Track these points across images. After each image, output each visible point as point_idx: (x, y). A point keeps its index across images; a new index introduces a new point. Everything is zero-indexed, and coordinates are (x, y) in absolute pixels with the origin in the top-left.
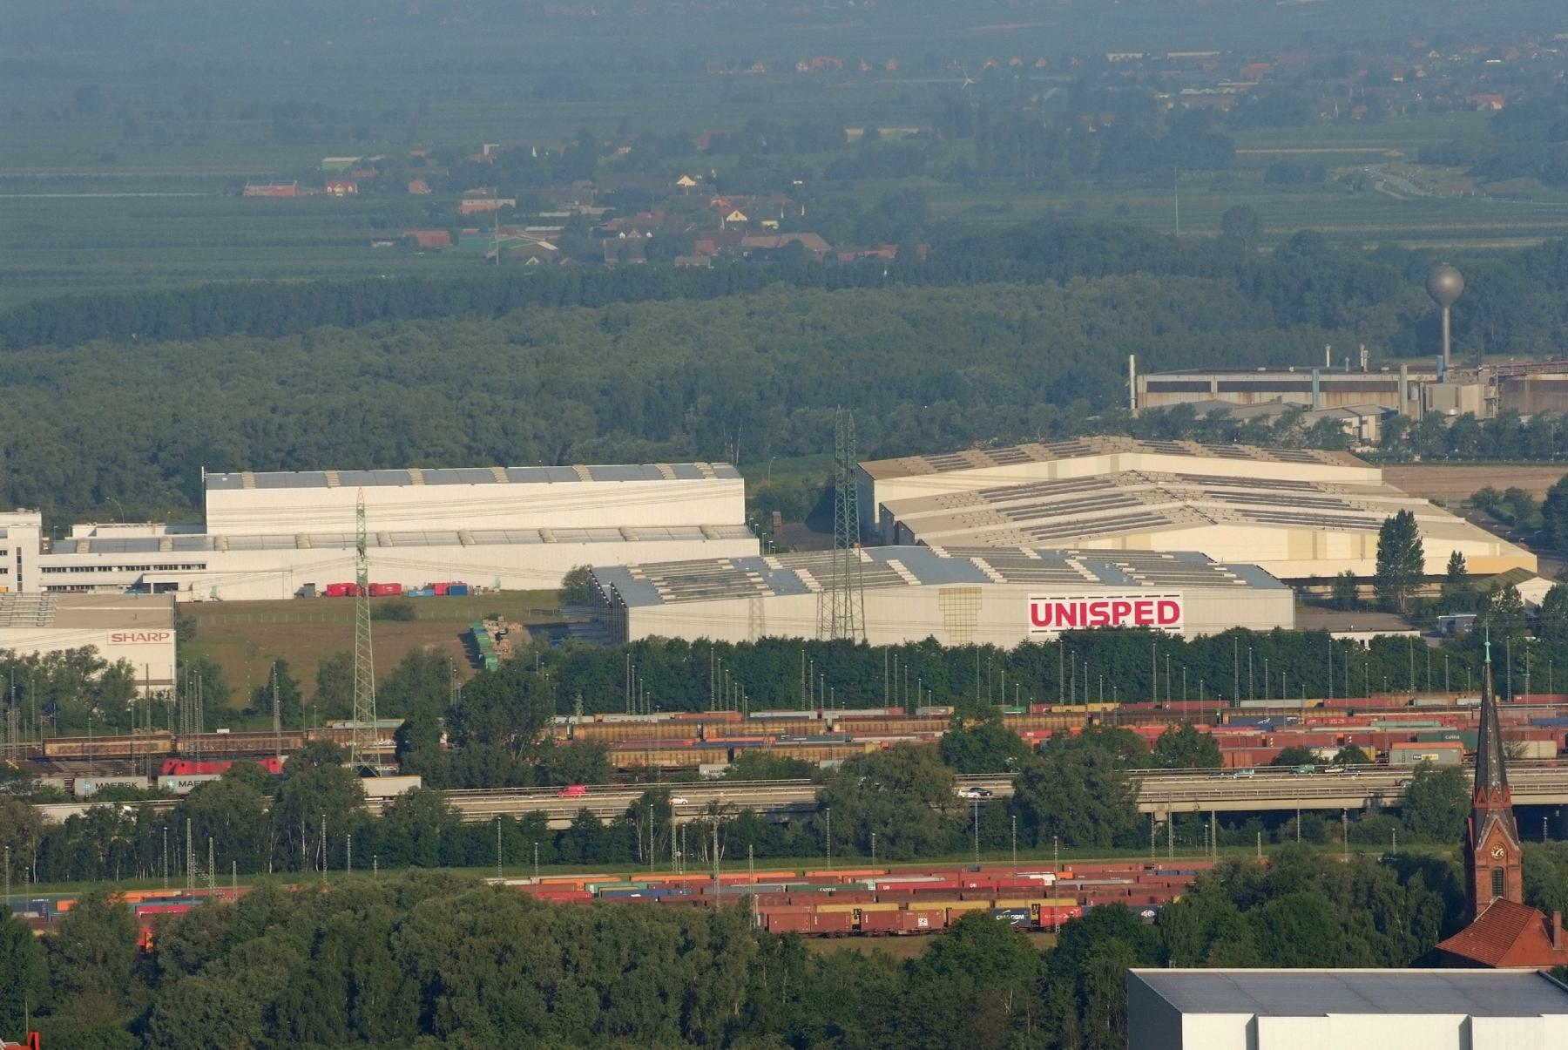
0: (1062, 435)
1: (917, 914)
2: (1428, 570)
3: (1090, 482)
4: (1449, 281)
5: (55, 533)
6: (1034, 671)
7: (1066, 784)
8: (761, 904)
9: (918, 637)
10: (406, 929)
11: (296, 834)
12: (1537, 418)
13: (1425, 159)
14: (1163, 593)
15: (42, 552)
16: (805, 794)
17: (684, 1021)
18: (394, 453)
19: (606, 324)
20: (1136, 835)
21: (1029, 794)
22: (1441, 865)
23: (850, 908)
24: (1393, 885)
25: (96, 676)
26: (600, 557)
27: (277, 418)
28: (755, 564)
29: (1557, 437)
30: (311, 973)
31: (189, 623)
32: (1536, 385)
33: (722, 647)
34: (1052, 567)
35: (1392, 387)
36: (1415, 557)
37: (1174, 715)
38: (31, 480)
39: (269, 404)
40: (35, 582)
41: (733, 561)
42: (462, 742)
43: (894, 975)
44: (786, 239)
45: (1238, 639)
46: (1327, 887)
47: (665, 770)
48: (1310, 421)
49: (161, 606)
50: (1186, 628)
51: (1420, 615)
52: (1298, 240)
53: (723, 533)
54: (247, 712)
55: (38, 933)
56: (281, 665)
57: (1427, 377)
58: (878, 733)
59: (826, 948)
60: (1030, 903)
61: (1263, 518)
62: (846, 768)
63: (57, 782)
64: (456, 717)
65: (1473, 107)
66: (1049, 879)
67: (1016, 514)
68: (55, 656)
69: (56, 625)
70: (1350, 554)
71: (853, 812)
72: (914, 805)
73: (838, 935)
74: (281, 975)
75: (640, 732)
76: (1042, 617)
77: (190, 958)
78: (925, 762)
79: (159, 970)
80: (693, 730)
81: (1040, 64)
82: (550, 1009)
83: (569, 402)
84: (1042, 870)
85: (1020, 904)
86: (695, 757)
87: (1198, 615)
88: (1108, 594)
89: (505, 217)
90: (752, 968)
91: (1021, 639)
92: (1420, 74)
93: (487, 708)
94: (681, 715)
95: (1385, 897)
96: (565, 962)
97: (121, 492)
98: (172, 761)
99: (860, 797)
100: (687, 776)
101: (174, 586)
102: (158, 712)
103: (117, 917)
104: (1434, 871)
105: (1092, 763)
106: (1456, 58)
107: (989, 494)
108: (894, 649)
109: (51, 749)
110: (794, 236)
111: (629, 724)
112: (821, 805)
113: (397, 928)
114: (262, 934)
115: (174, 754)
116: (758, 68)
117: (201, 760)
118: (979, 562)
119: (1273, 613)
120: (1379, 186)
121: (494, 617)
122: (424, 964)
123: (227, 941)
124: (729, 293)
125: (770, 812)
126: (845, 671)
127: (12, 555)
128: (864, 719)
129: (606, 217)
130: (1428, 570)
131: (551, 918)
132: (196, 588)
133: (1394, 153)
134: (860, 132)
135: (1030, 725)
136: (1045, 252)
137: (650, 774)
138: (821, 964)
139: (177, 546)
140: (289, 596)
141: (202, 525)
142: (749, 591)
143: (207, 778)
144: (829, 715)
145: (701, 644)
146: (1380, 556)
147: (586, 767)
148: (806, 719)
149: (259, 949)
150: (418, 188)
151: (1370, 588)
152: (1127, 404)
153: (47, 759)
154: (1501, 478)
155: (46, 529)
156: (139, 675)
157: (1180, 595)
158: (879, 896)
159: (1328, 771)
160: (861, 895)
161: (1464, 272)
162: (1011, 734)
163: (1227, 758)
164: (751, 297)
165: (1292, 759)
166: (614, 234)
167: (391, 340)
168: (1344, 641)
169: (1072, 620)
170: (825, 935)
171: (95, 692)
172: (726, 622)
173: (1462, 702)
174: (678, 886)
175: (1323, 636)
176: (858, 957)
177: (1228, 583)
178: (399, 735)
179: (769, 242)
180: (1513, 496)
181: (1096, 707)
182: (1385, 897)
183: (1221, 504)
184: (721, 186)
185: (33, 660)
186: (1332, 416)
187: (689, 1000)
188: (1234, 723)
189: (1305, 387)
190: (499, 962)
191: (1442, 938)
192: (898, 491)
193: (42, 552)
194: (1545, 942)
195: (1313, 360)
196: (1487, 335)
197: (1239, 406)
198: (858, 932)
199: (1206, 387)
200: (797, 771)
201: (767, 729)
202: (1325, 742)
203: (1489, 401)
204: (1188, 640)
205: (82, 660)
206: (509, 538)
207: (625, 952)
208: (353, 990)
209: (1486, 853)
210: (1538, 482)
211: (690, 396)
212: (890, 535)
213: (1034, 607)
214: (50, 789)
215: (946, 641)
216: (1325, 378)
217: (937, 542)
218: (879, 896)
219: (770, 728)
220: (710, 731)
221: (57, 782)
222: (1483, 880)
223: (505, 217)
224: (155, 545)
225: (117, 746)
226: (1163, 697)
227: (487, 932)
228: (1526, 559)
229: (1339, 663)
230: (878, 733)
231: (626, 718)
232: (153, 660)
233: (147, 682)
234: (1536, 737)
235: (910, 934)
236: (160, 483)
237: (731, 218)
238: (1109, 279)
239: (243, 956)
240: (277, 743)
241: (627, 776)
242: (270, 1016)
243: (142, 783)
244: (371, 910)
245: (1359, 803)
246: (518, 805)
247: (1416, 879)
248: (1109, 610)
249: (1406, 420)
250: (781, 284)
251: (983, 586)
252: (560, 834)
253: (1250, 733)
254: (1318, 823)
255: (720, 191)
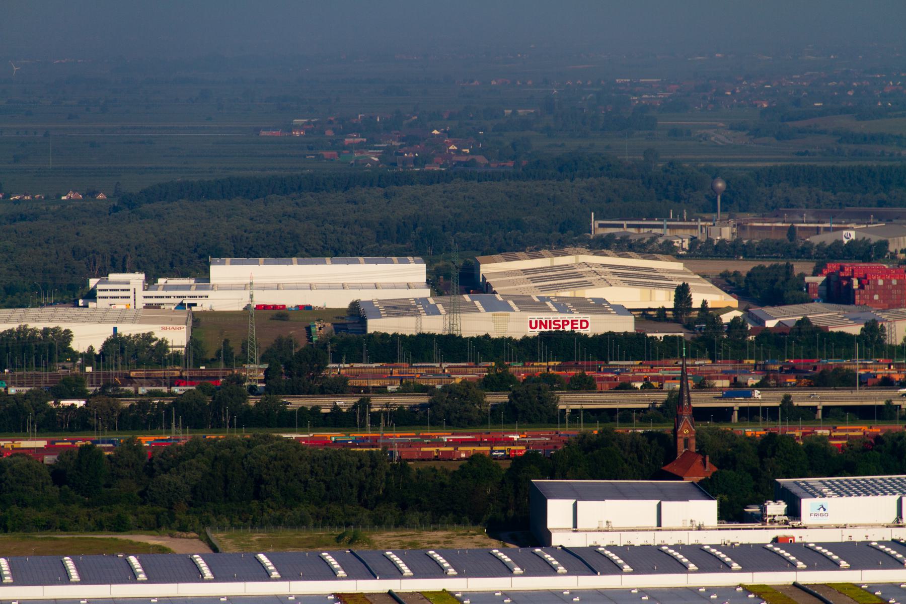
0: (559, 246)
1: (461, 452)
2: (694, 306)
3: (566, 267)
4: (720, 185)
5: (150, 282)
6: (527, 348)
7: (529, 398)
8: (399, 447)
9: (482, 334)
10: (249, 457)
11: (220, 414)
12: (750, 242)
13: (731, 129)
14: (582, 317)
15: (144, 290)
16: (425, 399)
17: (359, 496)
18: (293, 249)
19: (386, 195)
20: (556, 418)
21: (514, 401)
22: (666, 436)
23: (434, 449)
24: (646, 444)
25: (153, 344)
26: (364, 296)
27: (246, 235)
28: (424, 301)
29: (758, 249)
30: (211, 474)
31: (199, 322)
32: (752, 228)
33: (403, 336)
34: (541, 305)
35: (696, 227)
36: (689, 301)
37: (581, 367)
38: (145, 259)
39: (243, 228)
40: (141, 303)
41: (415, 299)
42: (291, 376)
43: (448, 478)
44: (470, 157)
45: (610, 337)
46: (620, 444)
47: (373, 387)
48: (661, 240)
49: (183, 315)
50: (590, 332)
51: (689, 326)
52: (671, 163)
53: (417, 286)
54: (213, 360)
55: (107, 453)
56: (226, 342)
57: (709, 223)
58: (461, 374)
59: (423, 466)
60: (507, 448)
61: (632, 284)
62: (444, 389)
63: (131, 389)
64: (288, 366)
65: (756, 106)
66: (516, 437)
67: (534, 280)
68: (138, 336)
69: (140, 323)
70: (664, 299)
71: (443, 408)
72: (468, 406)
73: (429, 460)
74: (199, 475)
75: (365, 372)
76: (534, 326)
77: (165, 467)
78: (473, 387)
79: (154, 471)
80: (388, 371)
81: (589, 83)
82: (306, 490)
83: (365, 229)
84: (514, 434)
85: (502, 448)
86: (387, 382)
87: (596, 325)
88: (560, 317)
89: (360, 147)
90: (388, 475)
91: (523, 335)
92: (738, 91)
93: (301, 363)
94: (385, 364)
95: (642, 448)
96: (312, 472)
97: (181, 263)
98: (179, 381)
99: (447, 402)
100: (381, 391)
101: (195, 305)
102: (176, 358)
103: (137, 449)
104: (660, 437)
105: (539, 389)
106: (754, 84)
107: (525, 271)
108: (472, 338)
109: (133, 374)
110: (474, 157)
111: (363, 368)
112: (431, 404)
113: (246, 457)
114: (193, 458)
115: (181, 377)
116: (476, 83)
117: (191, 381)
118: (511, 303)
119: (626, 325)
120: (713, 138)
121: (319, 320)
122: (256, 471)
123: (182, 459)
124: (438, 182)
125: (411, 407)
126: (451, 347)
127: (132, 291)
128: (458, 367)
129: (401, 147)
130: (694, 306)
131: (308, 454)
132: (203, 305)
133: (721, 124)
134: (510, 111)
135: (519, 370)
136: (568, 167)
137: (367, 390)
138: (419, 472)
139: (197, 289)
140: (241, 309)
141: (208, 280)
142: (416, 314)
143: (191, 388)
144: (444, 365)
145: (395, 335)
146: (675, 300)
147: (338, 387)
148: (434, 367)
149: (191, 464)
150: (329, 133)
151: (670, 312)
152: (590, 232)
153: (132, 378)
154: (744, 267)
155: (147, 279)
156: (170, 344)
157: (589, 317)
158: (448, 444)
159: (635, 393)
160: (440, 443)
161: (728, 182)
162: (512, 376)
163: (599, 386)
164: (446, 185)
165: (625, 387)
166: (402, 154)
167: (299, 201)
168: (652, 338)
169: (546, 327)
170: (423, 460)
171: (152, 350)
172: (406, 326)
173: (697, 363)
174: (367, 438)
175: (644, 335)
176: (434, 470)
177: (609, 313)
178: (266, 372)
179: (463, 159)
180: (736, 274)
181: (551, 363)
182: (642, 448)
183: (616, 277)
184: (449, 134)
185: (129, 337)
186: (669, 239)
187: (361, 488)
188: (606, 371)
189: (661, 227)
190: (285, 471)
191: (664, 465)
192: (490, 269)
193: (144, 290)
194: (702, 468)
195: (664, 216)
196: (740, 205)
197: (634, 234)
198: (437, 458)
199: (622, 226)
200: (424, 390)
201: (419, 372)
202: (638, 379)
203: (733, 234)
204: (590, 336)
205: (148, 337)
206: (330, 287)
207: (336, 468)
208: (226, 481)
209: (682, 432)
210: (744, 267)
211: (416, 226)
212: (485, 289)
213: (531, 322)
214: (128, 391)
215: (494, 335)
216: (669, 223)
217: (501, 290)
218: (448, 444)
219: (420, 371)
220: (395, 371)
221: (131, 389)
222: (680, 442)
223: (360, 147)
224: (188, 288)
225: (159, 373)
226: (578, 360)
227: (281, 459)
228: (733, 302)
229: (648, 345)
230: (461, 374)
231: (362, 365)
232: (177, 337)
233: (172, 347)
234: (722, 378)
235: (458, 460)
236: (197, 261)
237: (451, 148)
238: (591, 179)
239: (184, 466)
240: (220, 373)
241: (356, 390)
242: (194, 491)
243: (165, 390)
244: (237, 448)
245: (647, 406)
246: (308, 402)
247: (655, 442)
248: (561, 323)
249: (699, 242)
250: (459, 179)
251: (511, 313)
252: (326, 414)
253: (610, 375)
254: (626, 415)
255: (449, 136)
